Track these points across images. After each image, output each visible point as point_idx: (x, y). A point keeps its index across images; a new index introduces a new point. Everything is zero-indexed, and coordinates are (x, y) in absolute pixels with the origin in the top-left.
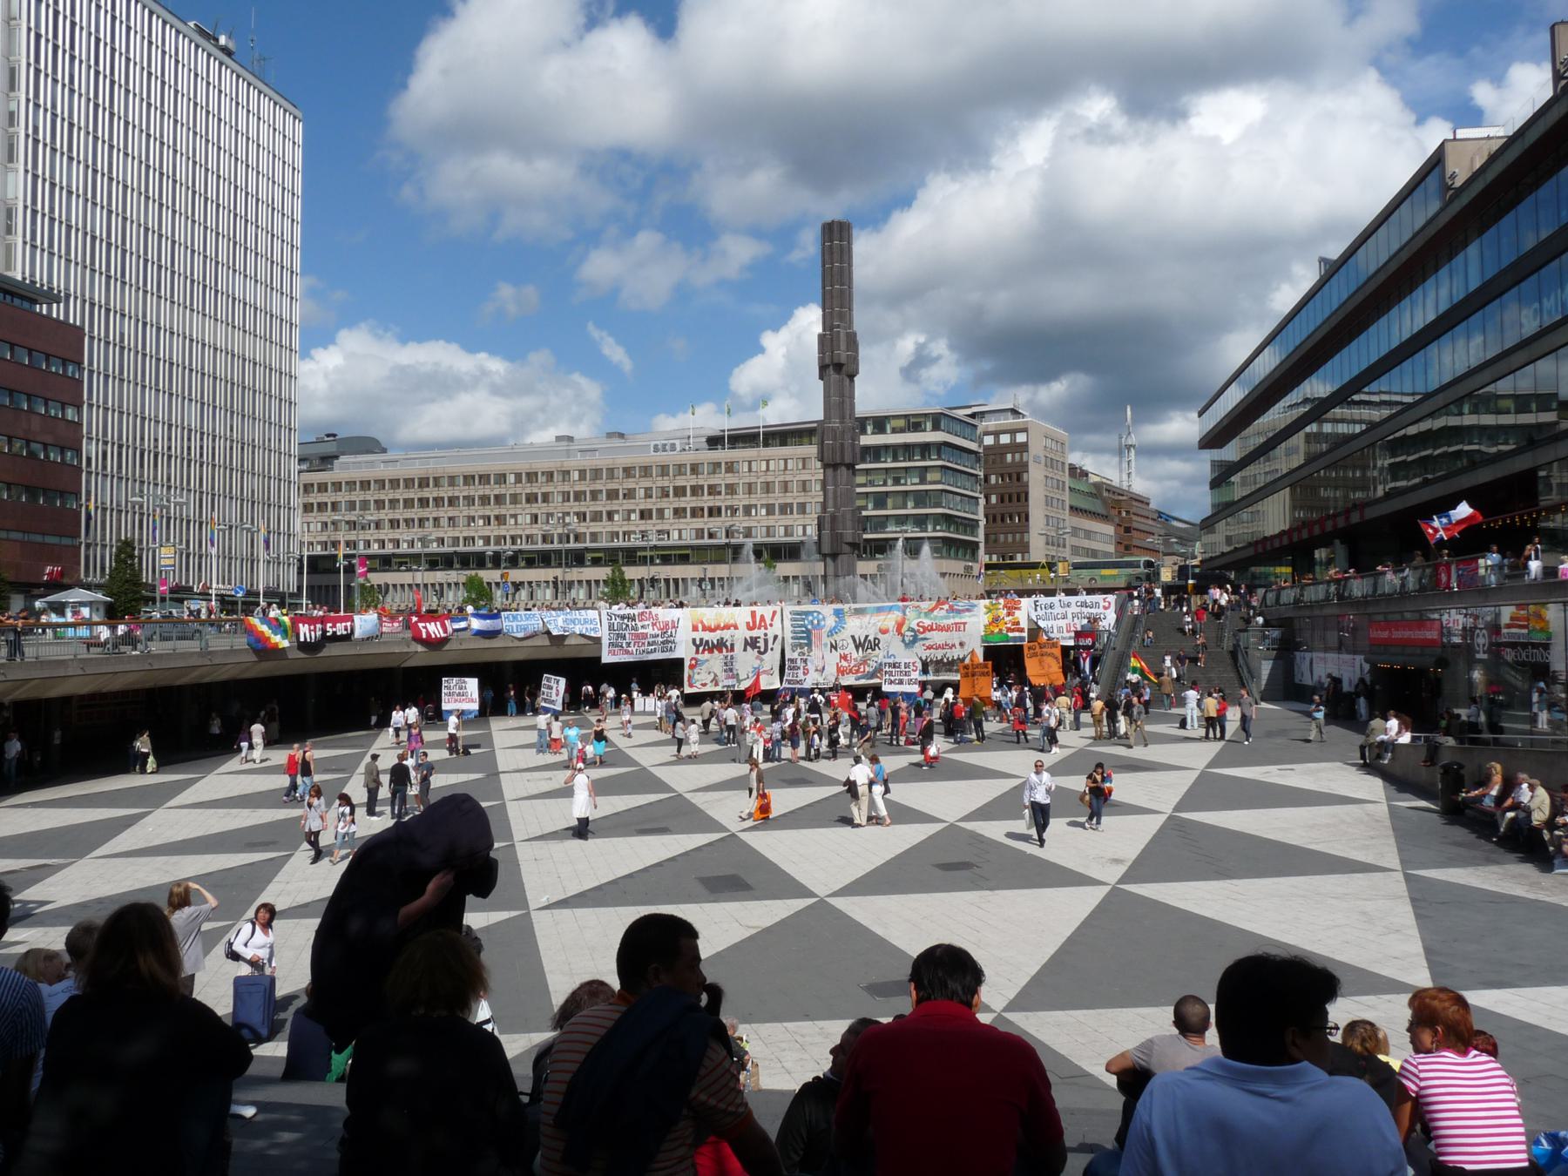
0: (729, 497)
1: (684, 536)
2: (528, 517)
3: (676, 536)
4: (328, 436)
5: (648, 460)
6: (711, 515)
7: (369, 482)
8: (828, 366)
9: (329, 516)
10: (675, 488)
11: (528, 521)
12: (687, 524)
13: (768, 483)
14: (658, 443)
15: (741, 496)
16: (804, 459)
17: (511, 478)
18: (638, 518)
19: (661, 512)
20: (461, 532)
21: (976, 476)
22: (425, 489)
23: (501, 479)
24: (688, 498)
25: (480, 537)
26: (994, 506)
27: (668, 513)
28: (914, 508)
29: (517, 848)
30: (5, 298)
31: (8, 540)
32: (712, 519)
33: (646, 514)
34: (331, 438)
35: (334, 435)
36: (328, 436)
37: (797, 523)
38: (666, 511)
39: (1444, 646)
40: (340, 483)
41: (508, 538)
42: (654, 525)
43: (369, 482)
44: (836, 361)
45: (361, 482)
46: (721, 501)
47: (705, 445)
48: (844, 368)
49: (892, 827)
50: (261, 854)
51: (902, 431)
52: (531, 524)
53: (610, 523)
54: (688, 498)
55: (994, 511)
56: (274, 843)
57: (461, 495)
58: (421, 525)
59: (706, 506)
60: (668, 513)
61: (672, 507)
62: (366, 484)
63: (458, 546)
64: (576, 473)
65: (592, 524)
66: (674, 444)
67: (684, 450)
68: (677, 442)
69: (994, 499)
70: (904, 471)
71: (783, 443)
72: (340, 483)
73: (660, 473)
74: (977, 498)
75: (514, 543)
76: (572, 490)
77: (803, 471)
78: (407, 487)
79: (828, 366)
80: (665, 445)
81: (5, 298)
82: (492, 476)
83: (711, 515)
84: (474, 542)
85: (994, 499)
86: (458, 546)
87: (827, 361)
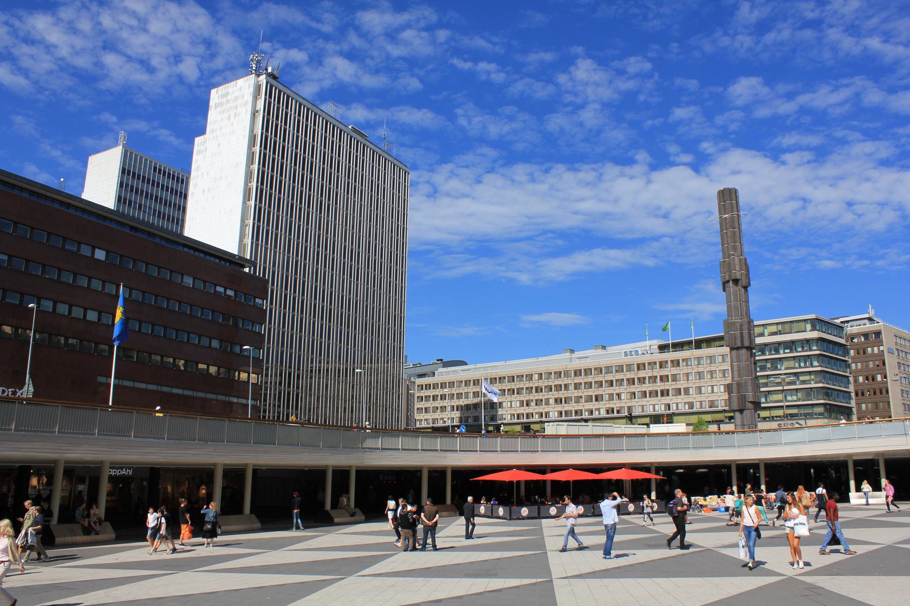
1: (645, 410)
2: (518, 403)
3: (675, 408)
4: (438, 360)
5: (620, 361)
7: (591, 370)
8: (728, 282)
9: (524, 397)
11: (518, 405)
14: (627, 350)
15: (682, 382)
17: (536, 377)
18: (534, 405)
19: (547, 400)
22: (589, 376)
24: (455, 400)
25: (536, 413)
26: (862, 384)
27: (552, 401)
31: (172, 387)
33: (665, 393)
34: (440, 362)
35: (441, 360)
36: (438, 360)
38: (551, 400)
39: (535, 503)
40: (645, 363)
41: (525, 414)
42: (472, 413)
43: (591, 370)
46: (669, 385)
47: (658, 351)
48: (740, 282)
50: (193, 541)
52: (520, 406)
53: (619, 401)
55: (862, 388)
57: (525, 387)
58: (528, 405)
60: (552, 401)
62: (493, 380)
63: (572, 416)
64: (537, 375)
65: (586, 404)
67: (643, 354)
68: (639, 350)
69: (861, 379)
70: (778, 360)
71: (708, 346)
75: (528, 418)
76: (573, 382)
77: (722, 364)
78: (586, 374)
79: (728, 282)
80: (631, 352)
83: (662, 395)
84: (533, 417)
85: (861, 379)
86: (572, 416)
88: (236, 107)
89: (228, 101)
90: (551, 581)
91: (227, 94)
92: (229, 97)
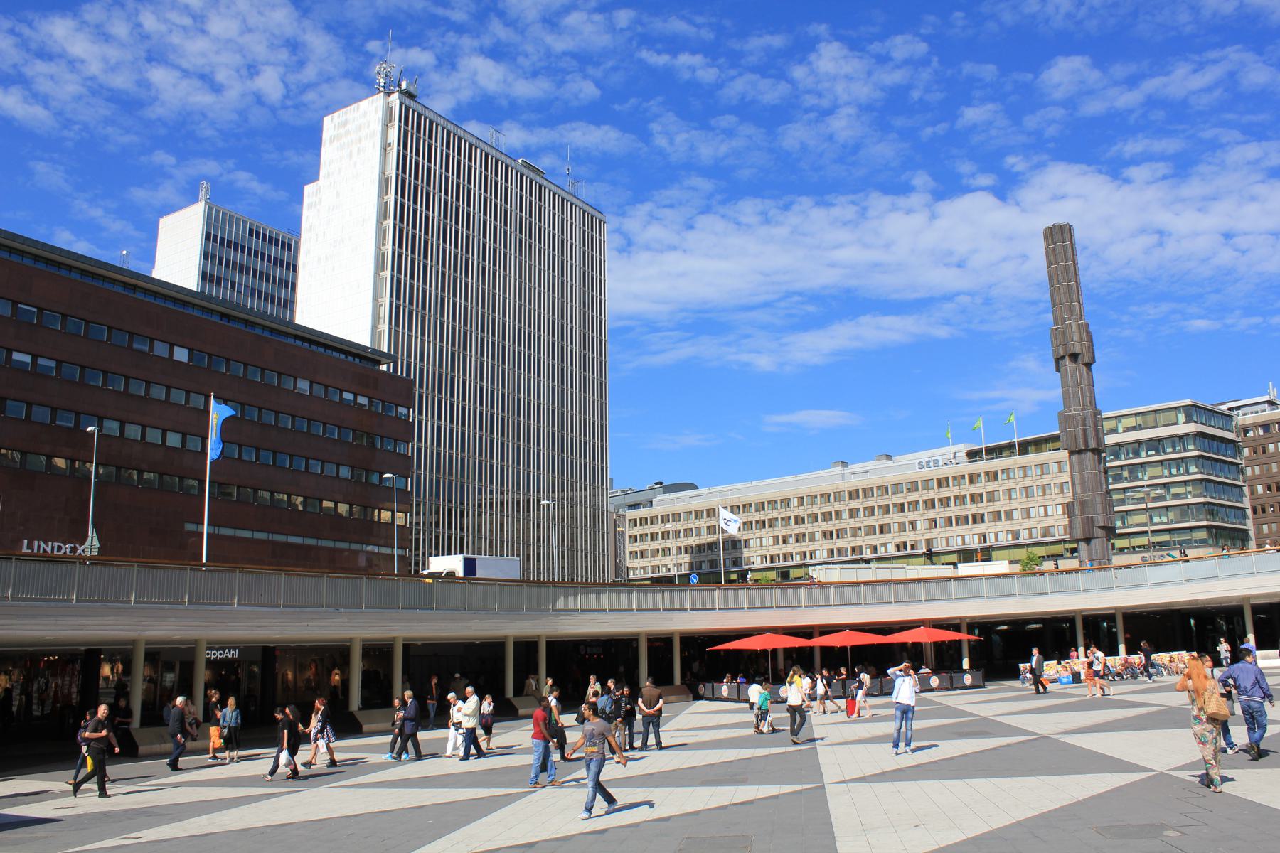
0: (991, 503)
1: (951, 543)
2: (771, 539)
6: (975, 521)
7: (872, 489)
8: (1063, 357)
9: (780, 531)
10: (940, 500)
11: (771, 543)
12: (954, 531)
13: (1026, 488)
14: (922, 460)
15: (1002, 502)
16: (1059, 463)
17: (795, 502)
19: (812, 534)
20: (807, 546)
21: (1237, 464)
23: (786, 503)
25: (797, 553)
26: (1261, 497)
27: (818, 536)
28: (1172, 500)
29: (818, 751)
30: (354, 360)
32: (976, 525)
37: (1023, 527)
38: (817, 534)
44: (1071, 352)
45: (696, 512)
46: (984, 508)
47: (966, 459)
49: (109, 775)
51: (1133, 429)
54: (953, 507)
56: (991, 734)
57: (779, 517)
59: (969, 514)
60: (818, 536)
61: (820, 530)
62: (676, 517)
63: (847, 556)
64: (796, 500)
66: (937, 460)
69: (1260, 489)
72: (948, 478)
73: (810, 502)
74: (1240, 487)
75: (785, 560)
77: (1059, 474)
79: (1063, 357)
80: (928, 462)
81: (354, 360)
82: (920, 483)
83: (975, 521)
86: (847, 556)
87: (1061, 353)
88: (360, 140)
89: (348, 133)
90: (823, 787)
91: (346, 123)
92: (349, 126)
